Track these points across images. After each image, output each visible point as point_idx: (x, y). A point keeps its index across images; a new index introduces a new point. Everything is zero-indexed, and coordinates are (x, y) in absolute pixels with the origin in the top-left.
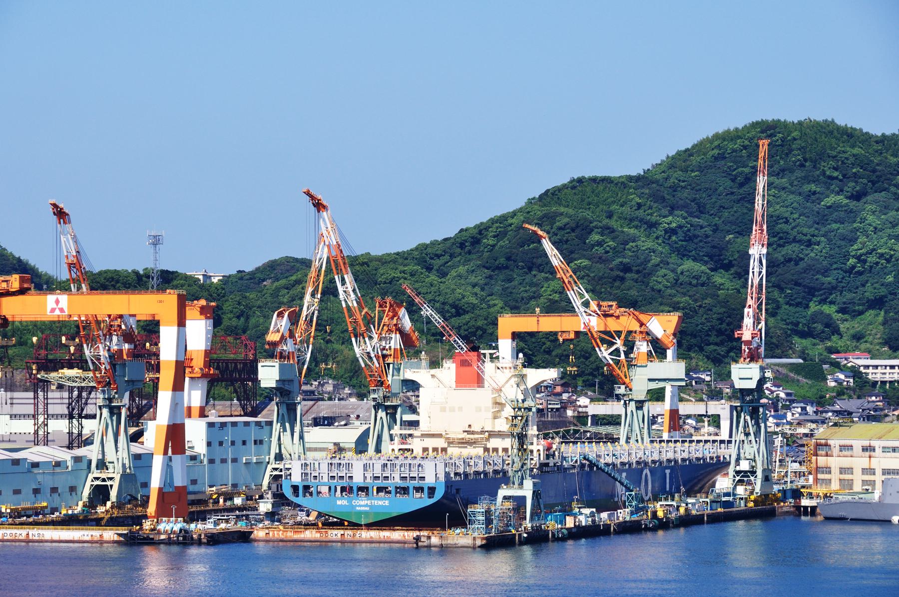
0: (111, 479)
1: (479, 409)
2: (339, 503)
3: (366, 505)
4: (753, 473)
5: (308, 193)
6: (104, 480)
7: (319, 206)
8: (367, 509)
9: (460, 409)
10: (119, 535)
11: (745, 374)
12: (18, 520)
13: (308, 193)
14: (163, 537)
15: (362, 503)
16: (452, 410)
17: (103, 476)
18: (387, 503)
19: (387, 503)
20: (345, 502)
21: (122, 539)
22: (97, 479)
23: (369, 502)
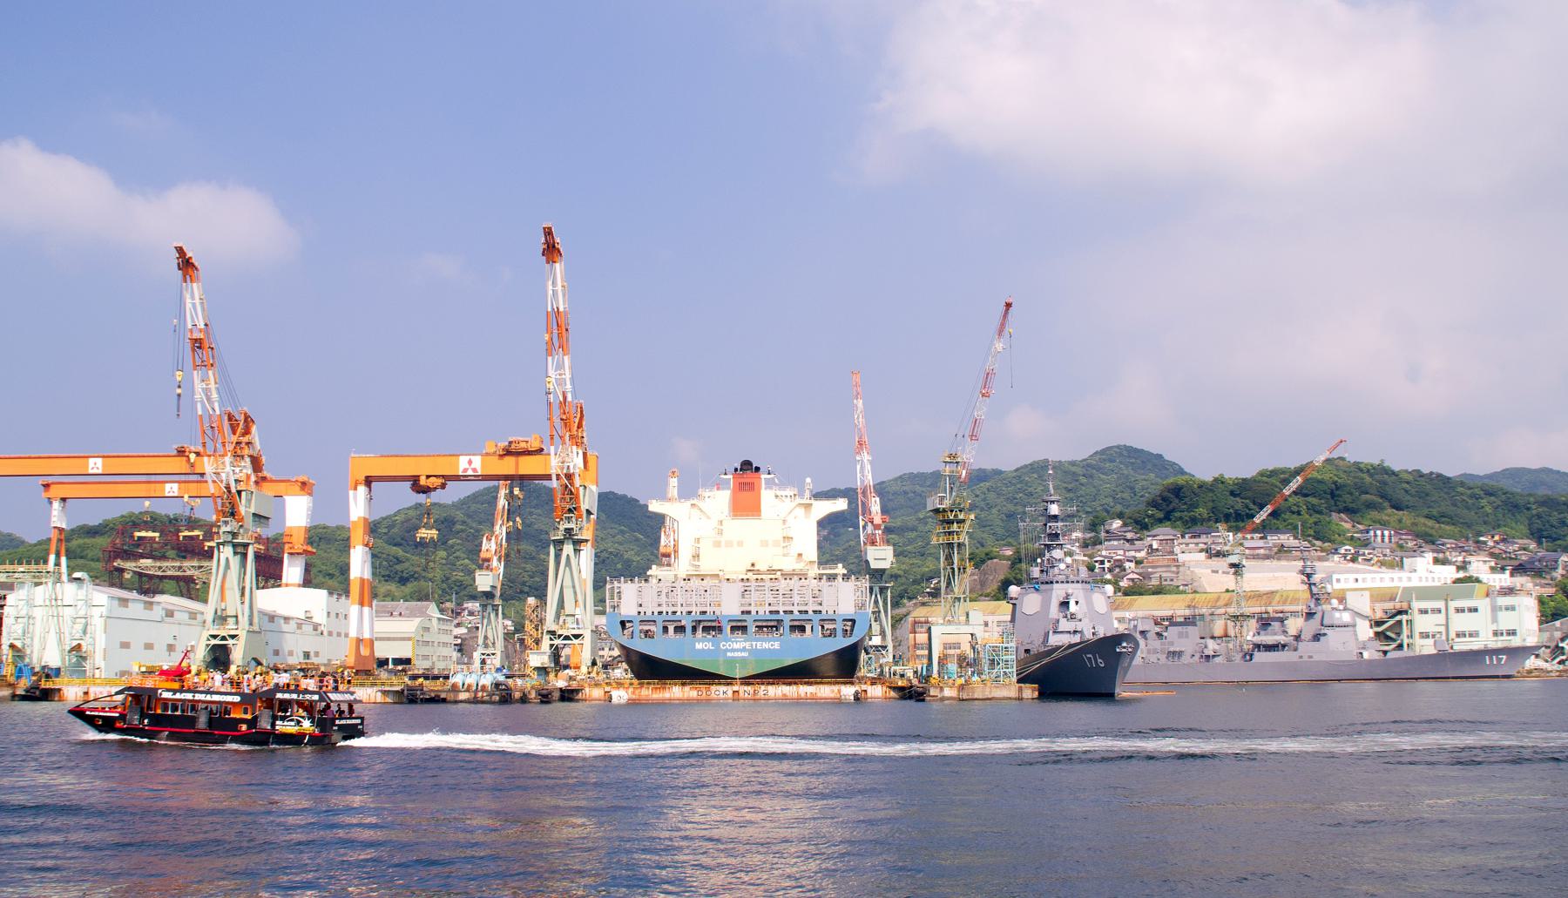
0: (233, 637)
1: (765, 544)
2: (699, 646)
3: (744, 649)
4: (884, 647)
5: (548, 232)
6: (224, 638)
7: (551, 250)
8: (745, 654)
9: (740, 544)
10: (385, 693)
11: (881, 554)
12: (249, 819)
13: (548, 232)
14: (463, 696)
15: (736, 646)
16: (729, 544)
17: (223, 633)
18: (777, 645)
19: (777, 645)
20: (709, 646)
21: (389, 700)
22: (215, 637)
23: (747, 645)
